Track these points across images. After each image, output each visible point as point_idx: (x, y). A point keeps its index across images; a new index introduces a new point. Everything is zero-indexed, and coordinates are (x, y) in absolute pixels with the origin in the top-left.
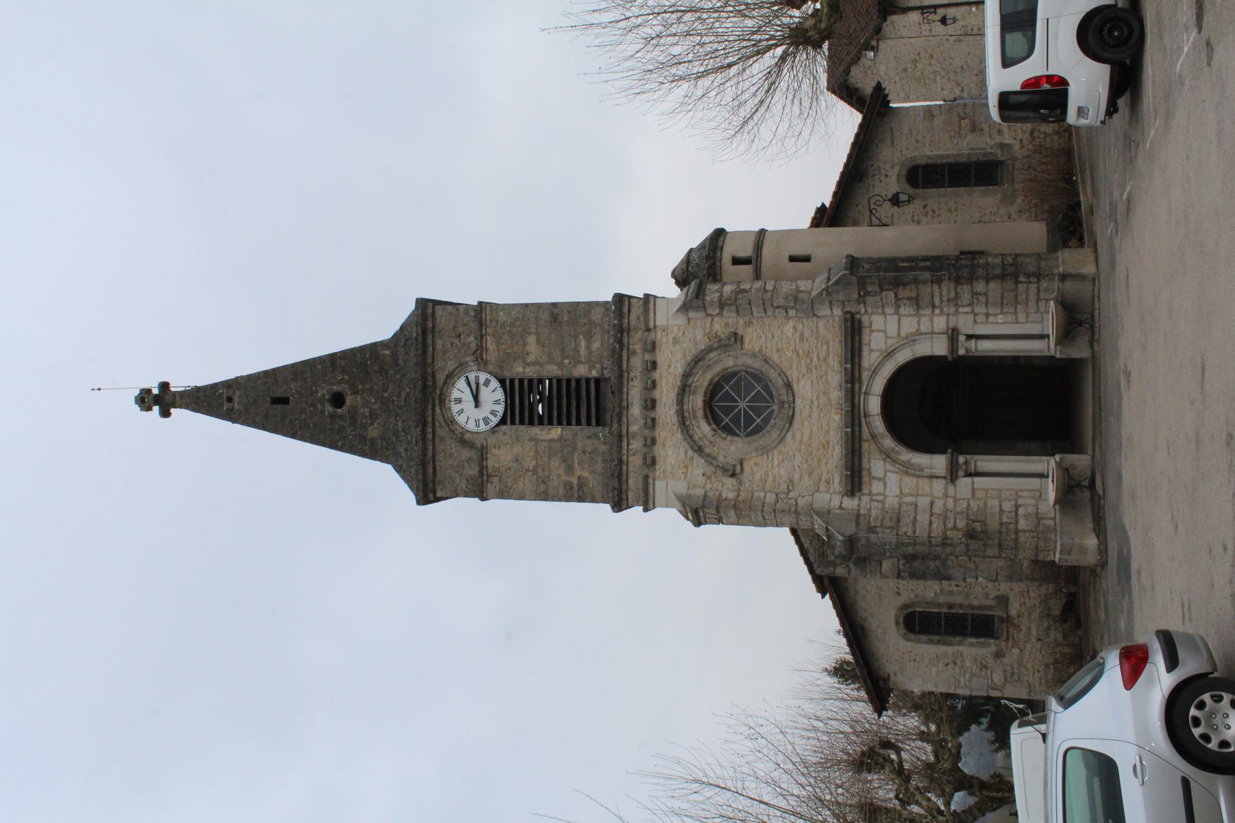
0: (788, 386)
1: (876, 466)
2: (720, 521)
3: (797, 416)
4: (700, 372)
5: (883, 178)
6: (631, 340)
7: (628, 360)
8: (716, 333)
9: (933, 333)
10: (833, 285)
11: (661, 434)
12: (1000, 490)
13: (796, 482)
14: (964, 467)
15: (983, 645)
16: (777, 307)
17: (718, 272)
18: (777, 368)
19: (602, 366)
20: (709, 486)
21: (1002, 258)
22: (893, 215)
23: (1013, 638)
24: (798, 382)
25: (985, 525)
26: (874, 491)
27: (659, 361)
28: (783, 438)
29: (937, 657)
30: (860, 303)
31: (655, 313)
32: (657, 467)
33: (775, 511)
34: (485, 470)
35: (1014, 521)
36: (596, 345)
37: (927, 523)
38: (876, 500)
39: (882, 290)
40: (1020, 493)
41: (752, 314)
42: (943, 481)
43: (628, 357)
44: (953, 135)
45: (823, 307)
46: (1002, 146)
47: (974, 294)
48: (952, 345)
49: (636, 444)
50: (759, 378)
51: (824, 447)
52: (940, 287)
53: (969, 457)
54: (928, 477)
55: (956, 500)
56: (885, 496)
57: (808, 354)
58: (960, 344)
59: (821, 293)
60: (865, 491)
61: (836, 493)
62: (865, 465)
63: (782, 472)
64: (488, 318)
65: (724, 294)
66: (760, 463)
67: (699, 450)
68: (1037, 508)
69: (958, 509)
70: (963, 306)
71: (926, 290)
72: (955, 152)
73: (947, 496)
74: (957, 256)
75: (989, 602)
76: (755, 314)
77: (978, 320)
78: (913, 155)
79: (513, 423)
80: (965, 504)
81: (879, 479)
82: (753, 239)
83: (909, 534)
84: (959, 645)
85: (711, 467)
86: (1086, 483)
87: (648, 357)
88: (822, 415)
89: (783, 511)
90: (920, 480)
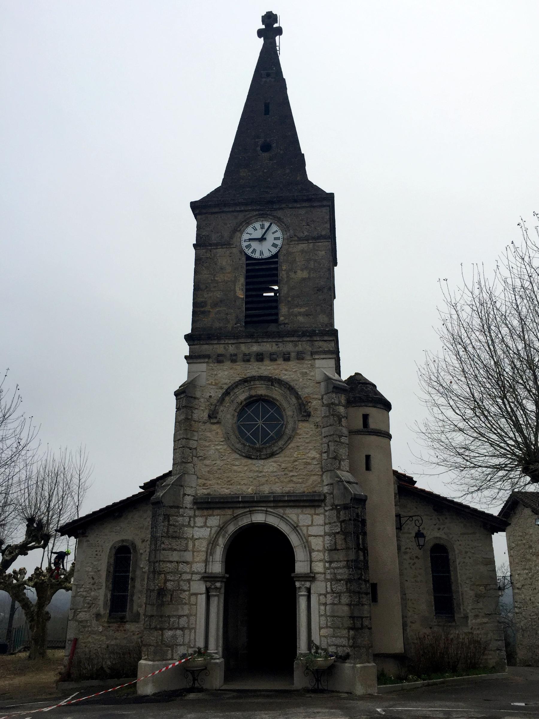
0: (272, 455)
1: (214, 521)
2: (178, 409)
3: (250, 461)
4: (282, 392)
5: (437, 526)
6: (304, 343)
7: (290, 341)
8: (310, 402)
9: (311, 562)
10: (344, 485)
11: (239, 367)
12: (196, 615)
13: (204, 462)
14: (213, 587)
15: (105, 604)
16: (328, 445)
17: (357, 405)
18: (285, 447)
19: (286, 324)
20: (202, 400)
21: (367, 617)
22: (410, 533)
23: (109, 627)
24: (275, 462)
25: (169, 604)
26: (197, 519)
27: (290, 363)
28: (235, 452)
29: (99, 571)
30: (332, 506)
31: (323, 359)
32: (216, 365)
33: (183, 447)
34: (215, 248)
35: (171, 626)
36: (301, 319)
37: (171, 559)
38: (190, 520)
39: (341, 522)
40: (193, 631)
41: (324, 427)
42: (204, 571)
43: (292, 341)
44: (473, 580)
45: (328, 478)
46: (466, 617)
47: (339, 594)
48: (302, 577)
49: (232, 349)
50: (280, 435)
51: (229, 481)
52: (344, 567)
53: (223, 591)
54: (206, 559)
55: (189, 581)
56: (193, 527)
57: (295, 468)
58: (303, 583)
59: (338, 477)
60: (197, 513)
61: (196, 491)
62: (217, 512)
63: (212, 452)
64: (320, 244)
65: (337, 407)
66: (218, 436)
67: (227, 393)
68: (180, 645)
69: (182, 583)
70: (331, 585)
71: (341, 555)
72: (459, 581)
73: (192, 574)
74: (368, 581)
75: (135, 608)
76: (323, 430)
77: (321, 597)
78: (456, 550)
79: (247, 265)
80: (185, 588)
81: (206, 522)
82: (382, 428)
83: (163, 546)
84: (106, 587)
85: (215, 401)
86: (197, 685)
87: (293, 355)
88: (251, 480)
89: (183, 453)
90: (204, 554)
